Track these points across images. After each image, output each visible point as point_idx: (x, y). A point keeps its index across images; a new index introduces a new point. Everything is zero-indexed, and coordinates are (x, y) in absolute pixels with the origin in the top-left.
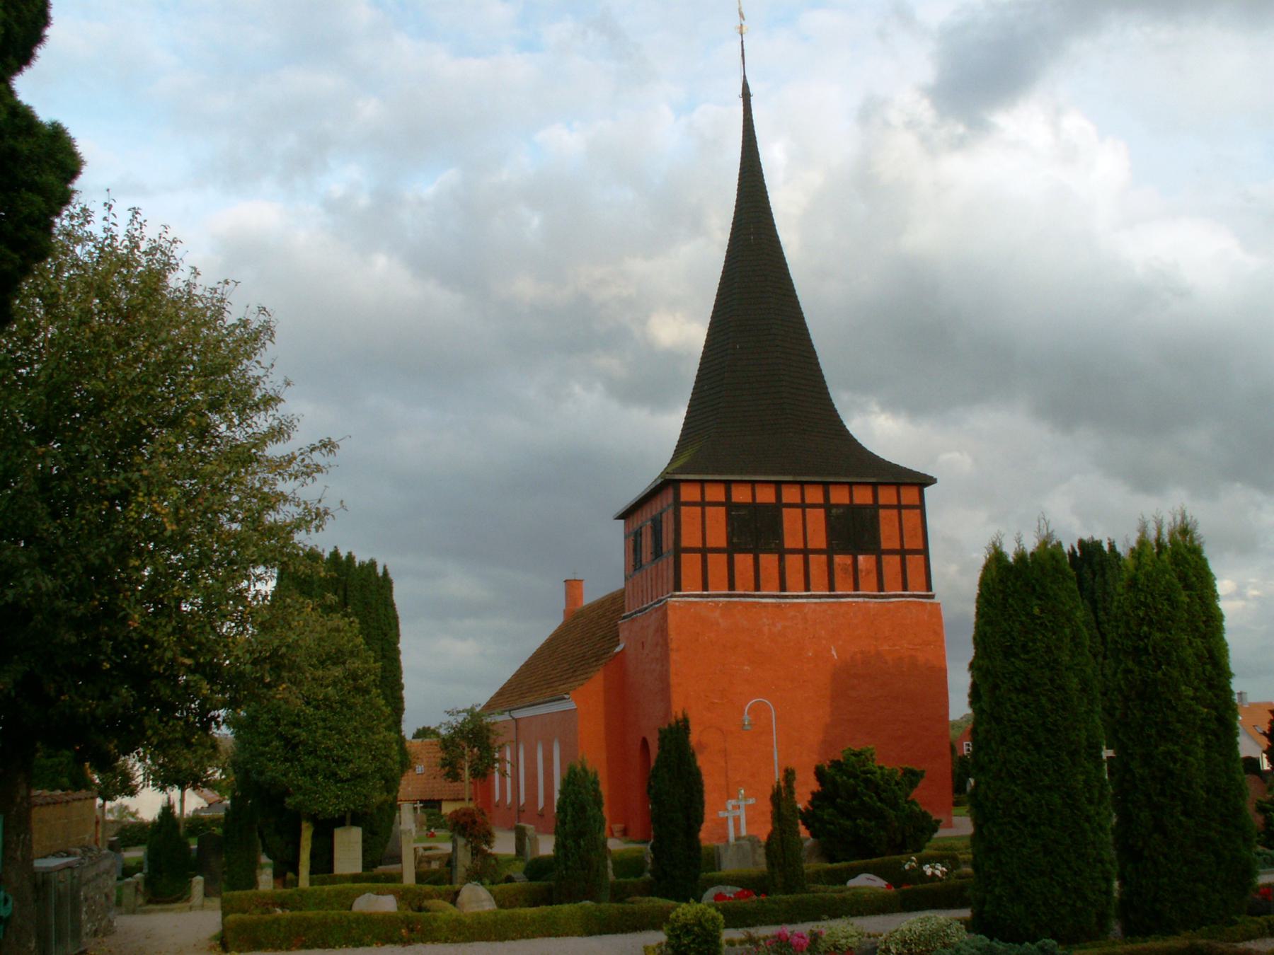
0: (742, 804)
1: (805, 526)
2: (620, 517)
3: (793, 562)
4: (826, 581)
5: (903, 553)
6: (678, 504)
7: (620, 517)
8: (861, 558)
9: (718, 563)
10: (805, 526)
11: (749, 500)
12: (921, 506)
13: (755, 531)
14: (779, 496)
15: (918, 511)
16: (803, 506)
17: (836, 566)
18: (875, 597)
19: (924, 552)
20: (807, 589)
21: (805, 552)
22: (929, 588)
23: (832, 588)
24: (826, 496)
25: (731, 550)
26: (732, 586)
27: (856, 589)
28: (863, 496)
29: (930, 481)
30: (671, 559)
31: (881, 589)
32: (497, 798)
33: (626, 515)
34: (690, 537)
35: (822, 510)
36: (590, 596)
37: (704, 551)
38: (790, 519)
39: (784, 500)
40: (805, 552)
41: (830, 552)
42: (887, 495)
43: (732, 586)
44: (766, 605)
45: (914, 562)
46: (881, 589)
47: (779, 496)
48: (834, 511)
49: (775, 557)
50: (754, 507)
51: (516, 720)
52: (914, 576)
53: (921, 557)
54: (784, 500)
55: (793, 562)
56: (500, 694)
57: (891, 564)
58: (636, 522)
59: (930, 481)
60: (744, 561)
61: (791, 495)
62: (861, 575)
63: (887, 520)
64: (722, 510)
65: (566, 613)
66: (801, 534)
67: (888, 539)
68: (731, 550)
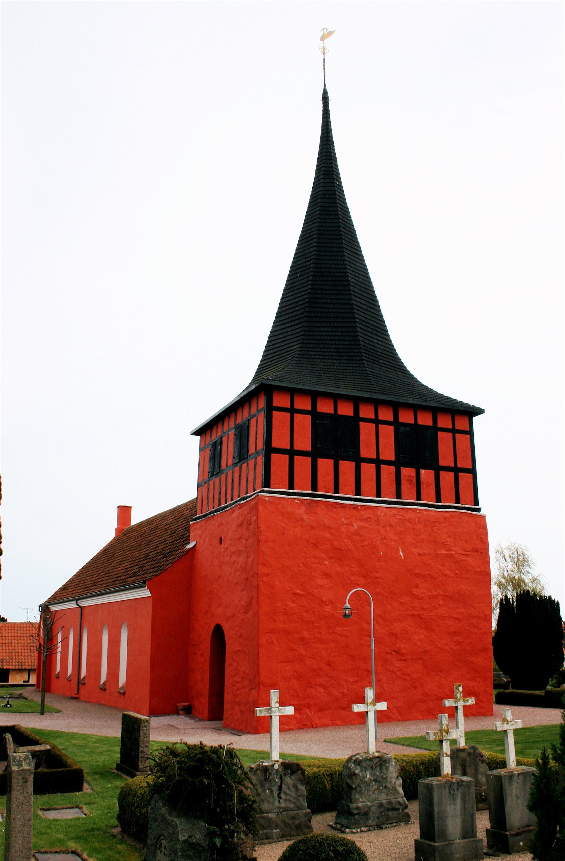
0: (460, 704)
1: (377, 440)
2: (196, 433)
3: (368, 470)
4: (394, 490)
5: (456, 470)
6: (270, 409)
7: (196, 433)
8: (423, 471)
9: (303, 465)
10: (377, 440)
11: (332, 412)
12: (470, 432)
13: (335, 440)
14: (356, 411)
15: (468, 436)
16: (377, 422)
17: (402, 476)
18: (434, 506)
19: (472, 471)
20: (379, 495)
21: (378, 462)
22: (477, 503)
23: (399, 496)
24: (396, 416)
25: (315, 454)
26: (314, 487)
27: (419, 498)
28: (425, 420)
29: (478, 411)
30: (261, 460)
31: (438, 500)
32: (58, 670)
33: (200, 432)
34: (280, 440)
35: (392, 428)
36: (136, 519)
37: (292, 453)
38: (366, 431)
39: (361, 415)
40: (378, 462)
41: (398, 464)
42: (444, 422)
43: (314, 487)
44: (343, 506)
45: (464, 478)
46: (337, 491)
47: (356, 411)
48: (402, 429)
49: (353, 464)
50: (335, 417)
51: (82, 608)
52: (465, 493)
53: (470, 476)
54: (361, 415)
55: (368, 470)
56: (64, 588)
57: (447, 478)
58: (214, 436)
59: (478, 411)
60: (325, 465)
61: (366, 412)
62: (423, 487)
63: (444, 439)
64: (309, 418)
65: (118, 531)
66: (374, 446)
67: (445, 459)
68: (315, 454)
